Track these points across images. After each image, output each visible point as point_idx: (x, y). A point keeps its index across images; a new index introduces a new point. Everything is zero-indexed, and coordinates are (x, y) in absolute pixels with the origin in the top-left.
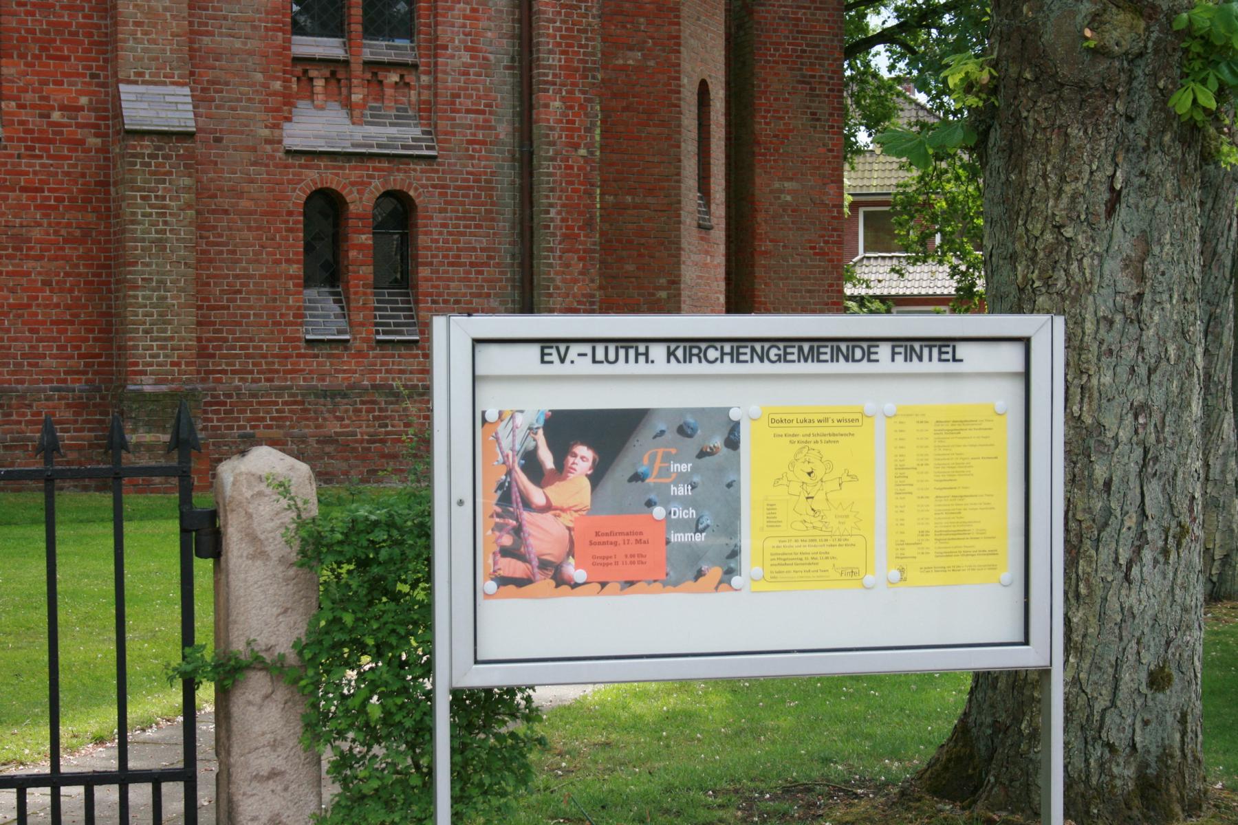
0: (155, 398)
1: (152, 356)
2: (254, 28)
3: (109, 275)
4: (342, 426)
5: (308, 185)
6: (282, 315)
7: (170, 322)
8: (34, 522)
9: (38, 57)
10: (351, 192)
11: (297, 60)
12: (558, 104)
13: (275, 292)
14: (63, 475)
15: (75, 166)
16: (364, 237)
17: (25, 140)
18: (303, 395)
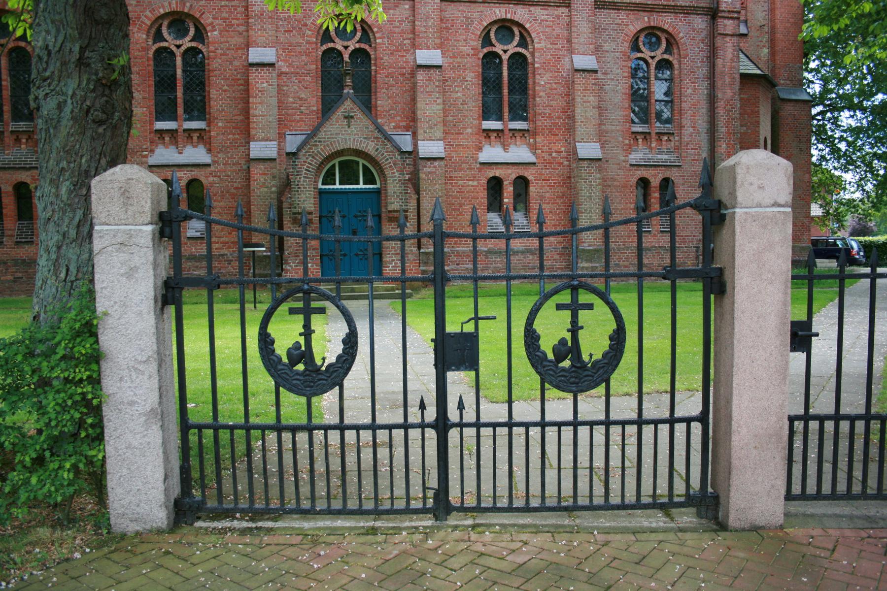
0: (589, 251)
8: (233, 302)
12: (724, 145)
14: (514, 278)
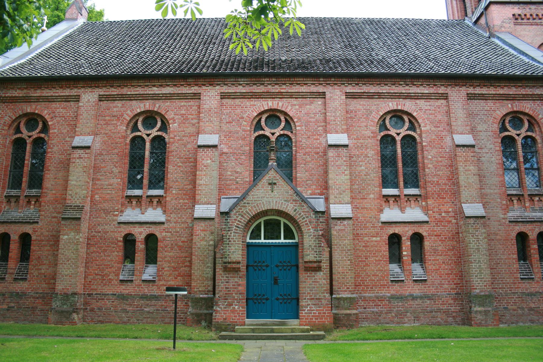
1: (478, 284)
2: (496, 186)
3: (461, 260)
4: (535, 305)
5: (516, 231)
6: (512, 270)
7: (483, 273)
9: (437, 198)
10: (529, 233)
11: (384, 196)
13: (510, 263)
15: (449, 228)
16: (535, 246)
17: (435, 221)
18: (522, 295)
